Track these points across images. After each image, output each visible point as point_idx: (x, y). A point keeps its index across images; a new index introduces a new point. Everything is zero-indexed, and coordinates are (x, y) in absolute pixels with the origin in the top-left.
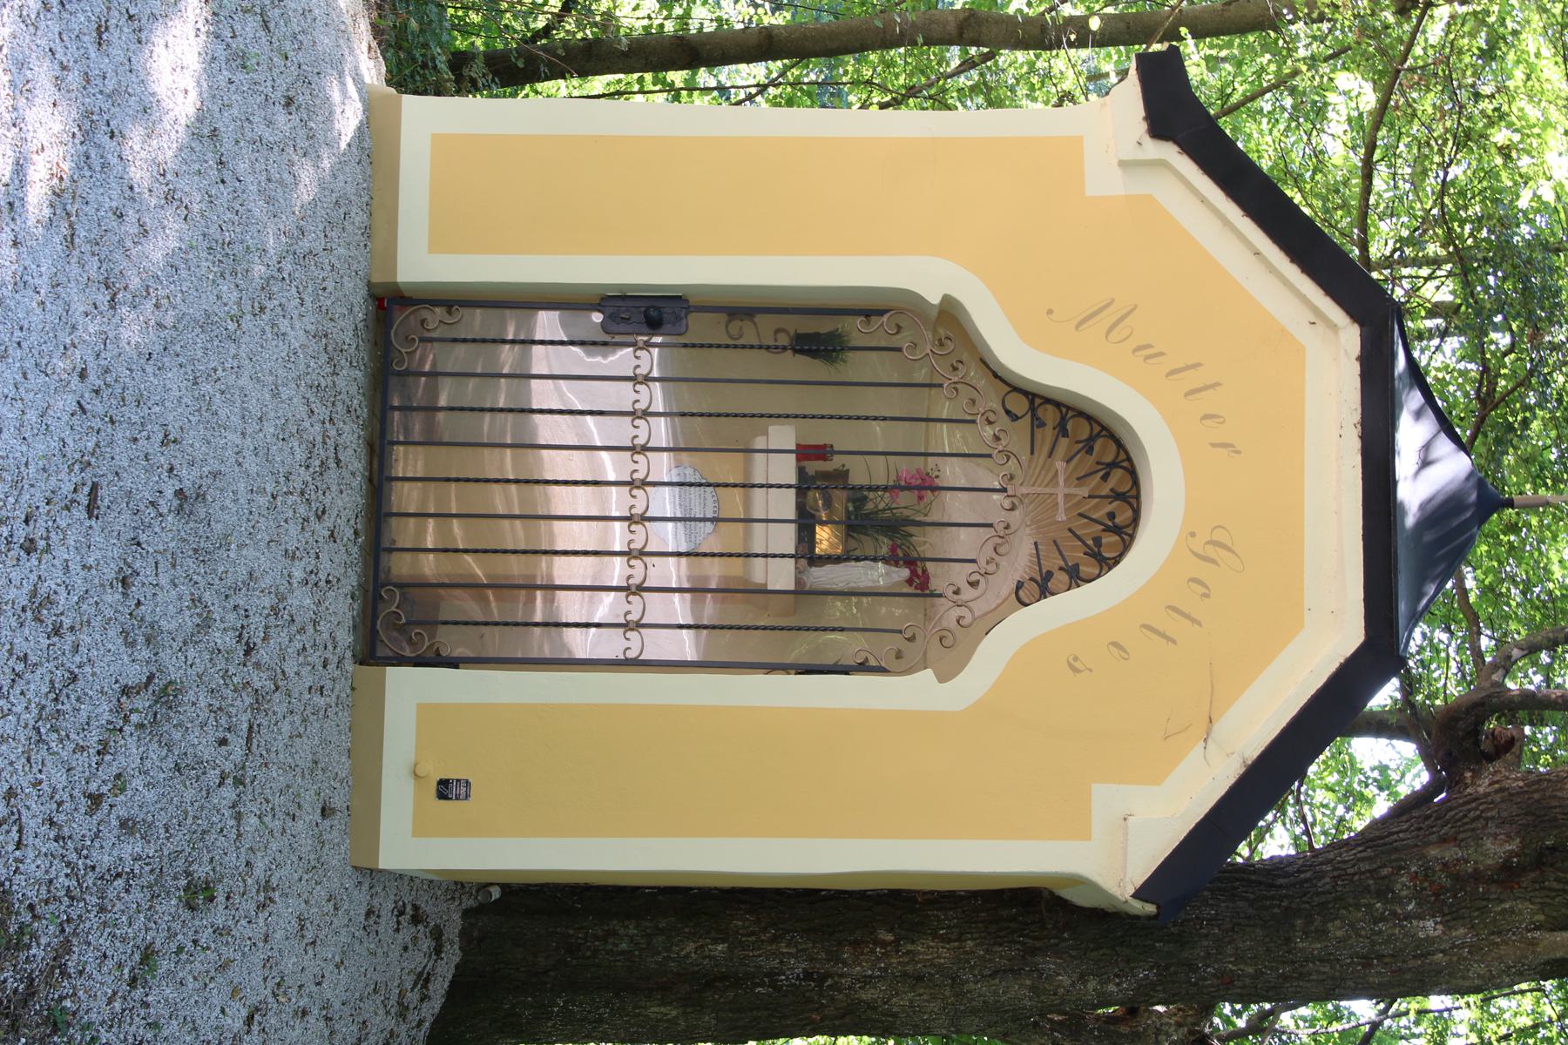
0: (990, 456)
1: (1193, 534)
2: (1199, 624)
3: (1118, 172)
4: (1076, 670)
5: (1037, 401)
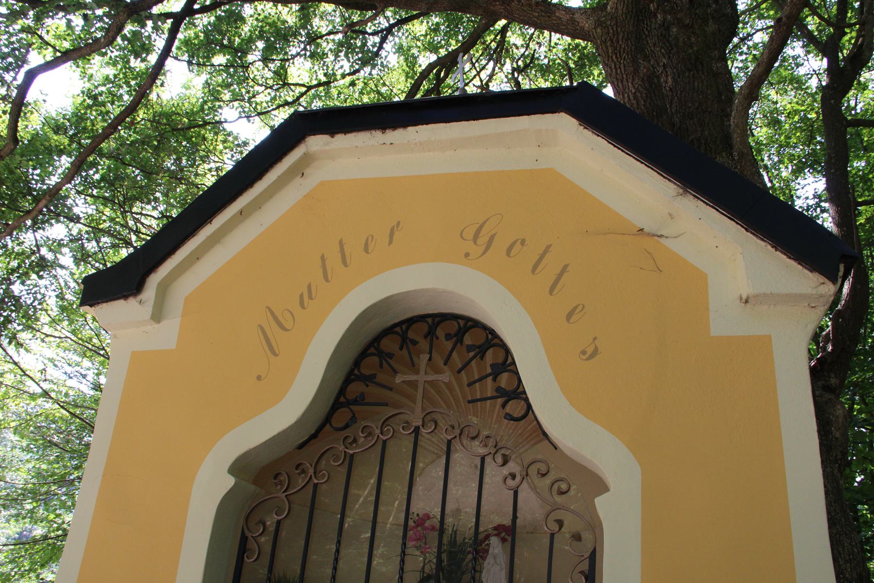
0: (385, 442)
1: (467, 255)
2: (549, 247)
3: (165, 323)
4: (595, 352)
5: (342, 399)
